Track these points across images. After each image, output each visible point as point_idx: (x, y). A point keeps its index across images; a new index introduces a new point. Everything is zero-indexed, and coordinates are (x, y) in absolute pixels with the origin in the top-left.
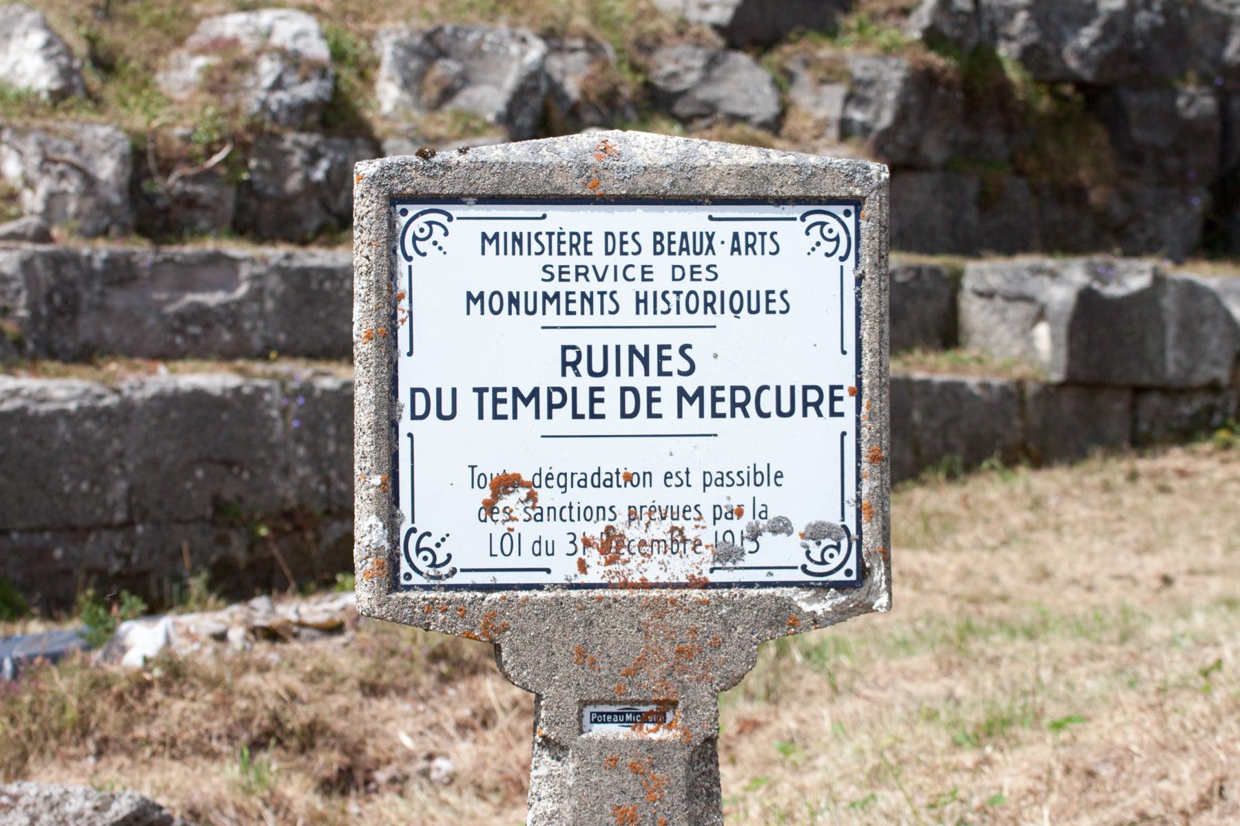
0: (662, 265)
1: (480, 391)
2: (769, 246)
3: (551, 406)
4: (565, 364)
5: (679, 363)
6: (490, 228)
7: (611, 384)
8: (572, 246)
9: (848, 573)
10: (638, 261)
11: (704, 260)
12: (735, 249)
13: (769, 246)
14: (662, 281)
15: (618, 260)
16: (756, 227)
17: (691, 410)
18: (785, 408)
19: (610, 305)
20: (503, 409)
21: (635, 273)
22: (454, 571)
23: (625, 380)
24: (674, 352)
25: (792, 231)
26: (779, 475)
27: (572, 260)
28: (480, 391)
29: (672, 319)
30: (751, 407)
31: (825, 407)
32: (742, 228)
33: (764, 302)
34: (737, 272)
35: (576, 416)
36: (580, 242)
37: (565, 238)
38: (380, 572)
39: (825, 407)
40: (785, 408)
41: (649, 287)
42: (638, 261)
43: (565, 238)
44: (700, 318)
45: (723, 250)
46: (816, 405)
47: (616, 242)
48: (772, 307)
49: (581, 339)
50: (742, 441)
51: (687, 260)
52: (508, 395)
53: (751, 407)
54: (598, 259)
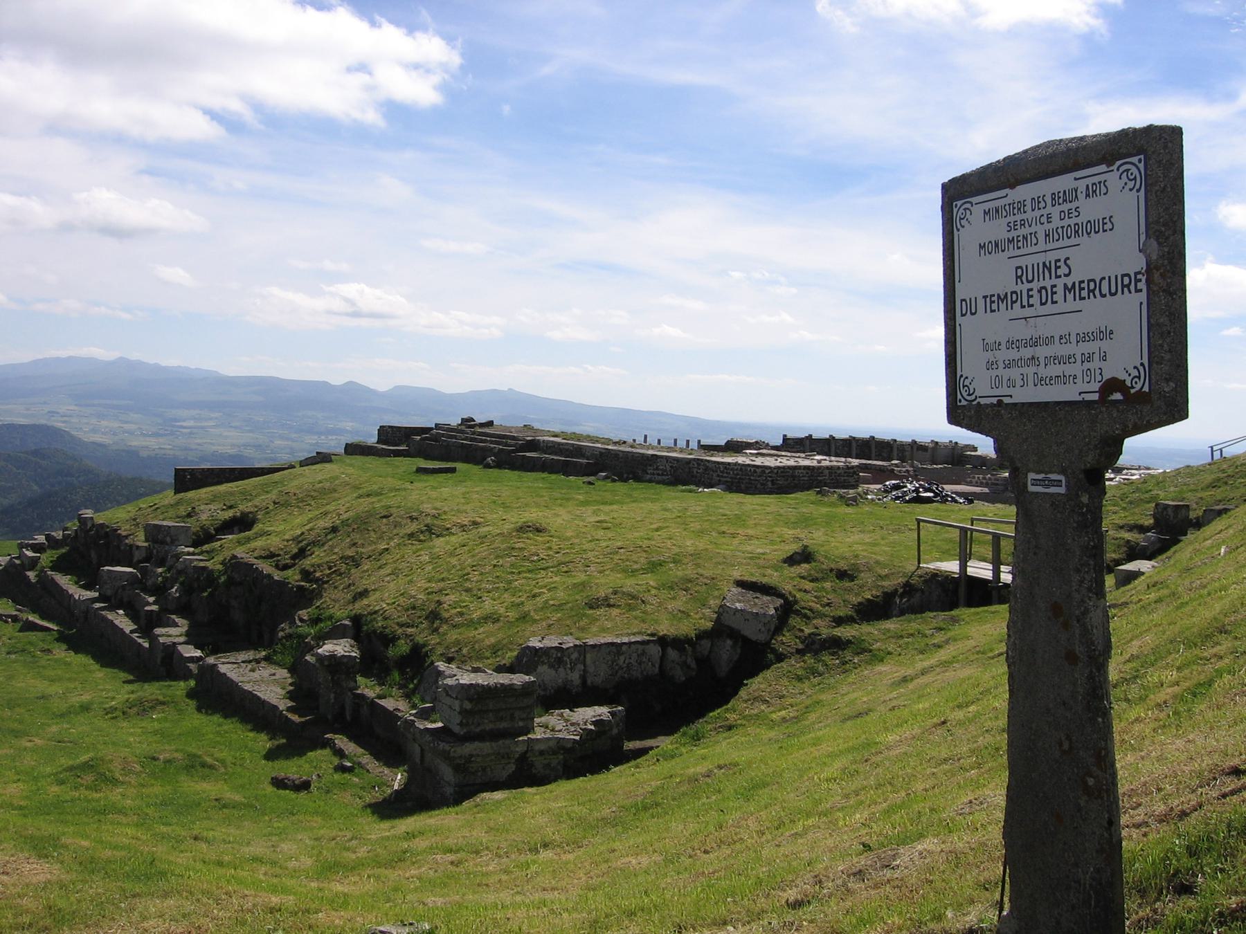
0: (1055, 212)
1: (985, 297)
2: (1104, 190)
3: (1013, 302)
4: (1017, 277)
5: (1064, 270)
6: (986, 206)
7: (1035, 286)
8: (1089, 291)
9: (1140, 161)
10: (1045, 212)
11: (1073, 205)
12: (1088, 195)
13: (1104, 190)
14: (1056, 222)
15: (1037, 213)
16: (1096, 179)
17: (1070, 296)
18: (1113, 290)
19: (1034, 241)
20: (995, 306)
21: (1044, 219)
22: (1142, 364)
23: (1042, 284)
24: (1061, 264)
25: (1113, 178)
26: (1111, 333)
27: (1018, 217)
28: (985, 297)
29: (1061, 244)
30: (1097, 292)
31: (1132, 287)
32: (1090, 181)
33: (1103, 226)
34: (1090, 209)
35: (1023, 307)
36: (1020, 206)
37: (1084, 285)
38: (693, 445)
39: (1132, 287)
40: (1113, 290)
41: (1050, 226)
42: (1045, 212)
43: (1084, 285)
44: (1073, 241)
45: (1082, 196)
46: (1128, 286)
47: (1037, 202)
48: (1106, 227)
49: (1022, 262)
50: (1095, 312)
51: (1065, 207)
52: (995, 298)
53: (1097, 292)
54: (1029, 215)
